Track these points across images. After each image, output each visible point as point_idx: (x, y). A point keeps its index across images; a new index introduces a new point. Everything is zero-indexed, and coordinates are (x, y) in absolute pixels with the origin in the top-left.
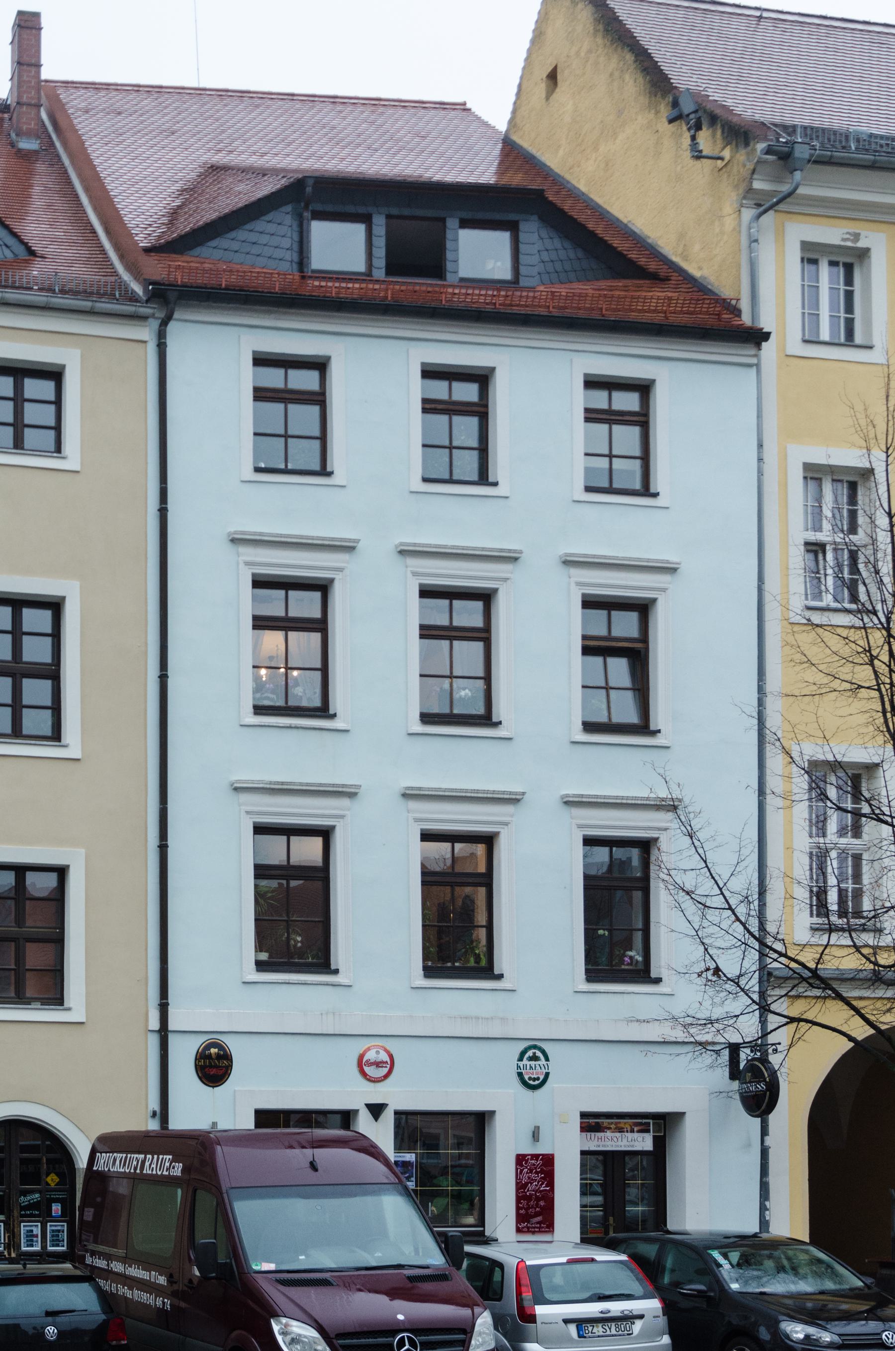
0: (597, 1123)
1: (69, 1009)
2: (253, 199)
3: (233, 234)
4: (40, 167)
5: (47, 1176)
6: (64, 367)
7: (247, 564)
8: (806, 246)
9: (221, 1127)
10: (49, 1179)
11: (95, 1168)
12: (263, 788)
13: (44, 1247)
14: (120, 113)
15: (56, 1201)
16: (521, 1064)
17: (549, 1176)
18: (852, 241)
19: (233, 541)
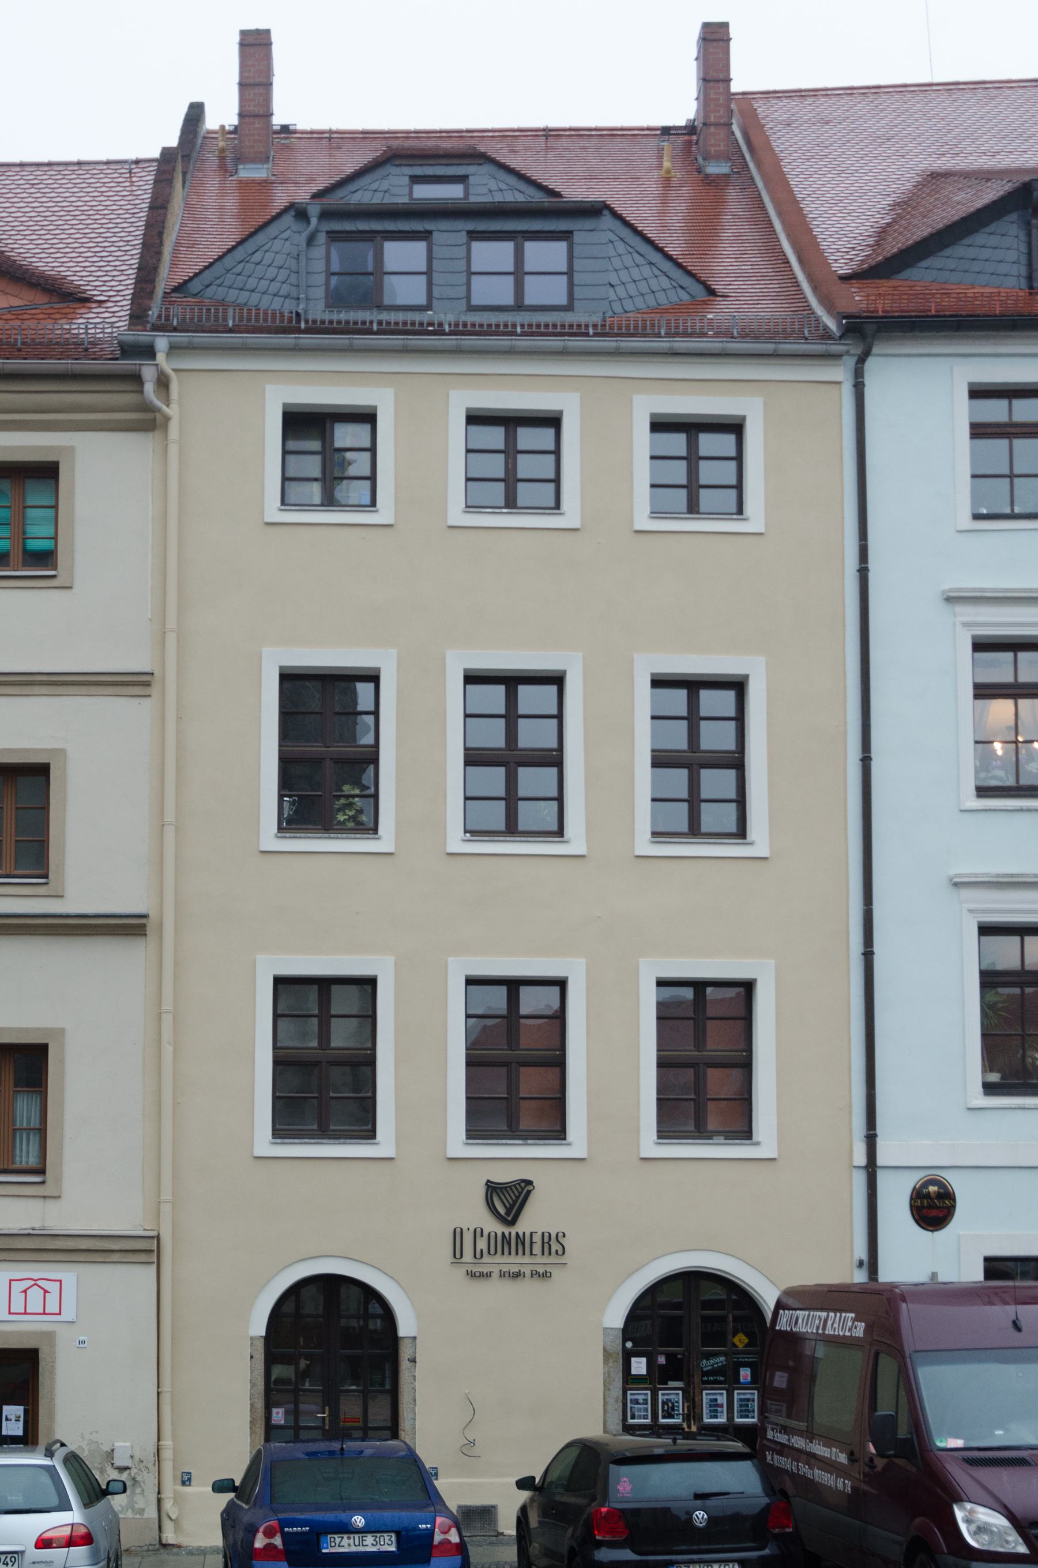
1: (758, 1144)
2: (972, 210)
3: (947, 252)
4: (732, 193)
5: (734, 1336)
6: (744, 418)
7: (966, 625)
9: (942, 1278)
10: (736, 1340)
11: (777, 1328)
12: (989, 883)
13: (730, 1418)
14: (827, 123)
15: (745, 1365)
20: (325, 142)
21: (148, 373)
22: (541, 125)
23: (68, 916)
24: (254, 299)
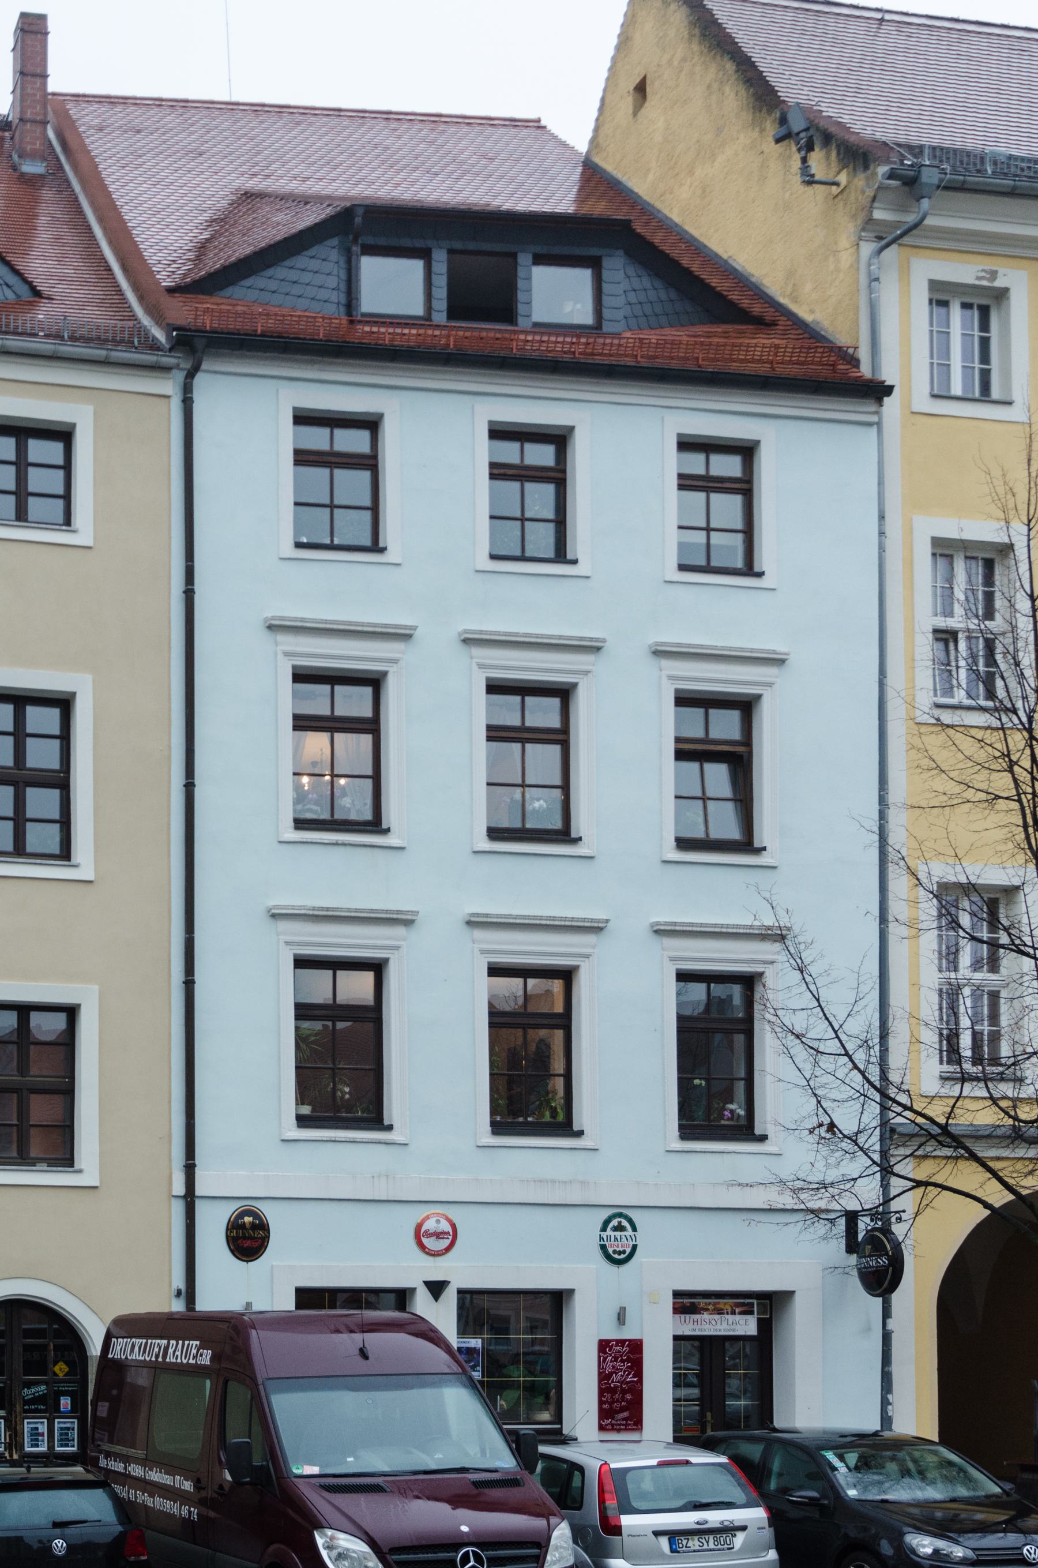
0: (693, 1304)
1: (80, 1171)
2: (294, 231)
3: (270, 272)
4: (47, 194)
5: (55, 1365)
6: (74, 425)
7: (287, 654)
8: (935, 285)
9: (256, 1308)
10: (57, 1369)
11: (110, 1356)
12: (305, 915)
13: (51, 1447)
14: (139, 132)
15: (65, 1393)
16: (604, 1235)
17: (636, 1365)
18: (989, 280)
19: (271, 627)
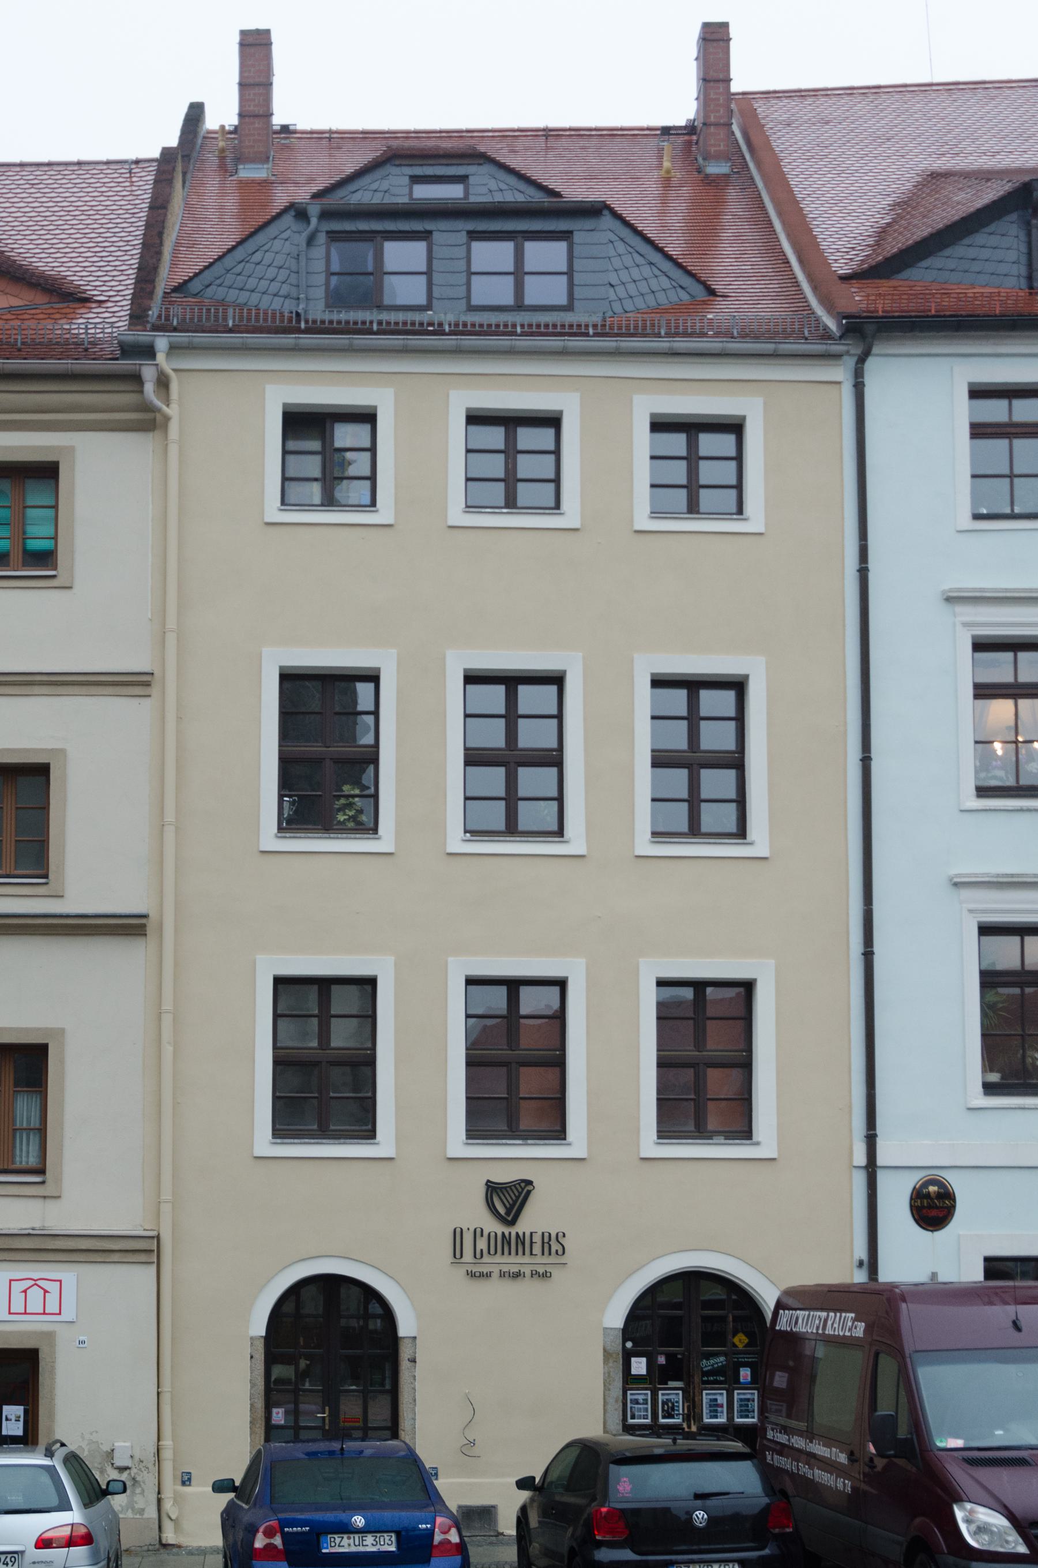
1: (758, 1144)
2: (972, 210)
3: (947, 252)
4: (732, 193)
5: (734, 1336)
6: (744, 418)
7: (966, 625)
9: (942, 1278)
10: (736, 1340)
11: (777, 1328)
12: (989, 883)
13: (730, 1418)
14: (827, 123)
15: (745, 1365)
20: (325, 142)
21: (148, 373)
22: (541, 125)
23: (68, 916)
24: (254, 299)
